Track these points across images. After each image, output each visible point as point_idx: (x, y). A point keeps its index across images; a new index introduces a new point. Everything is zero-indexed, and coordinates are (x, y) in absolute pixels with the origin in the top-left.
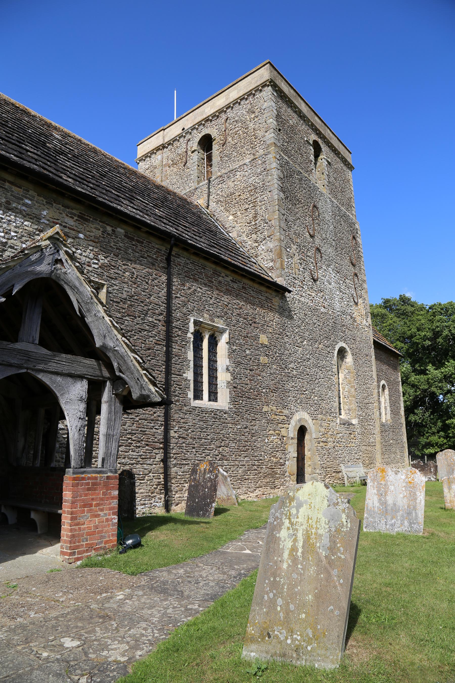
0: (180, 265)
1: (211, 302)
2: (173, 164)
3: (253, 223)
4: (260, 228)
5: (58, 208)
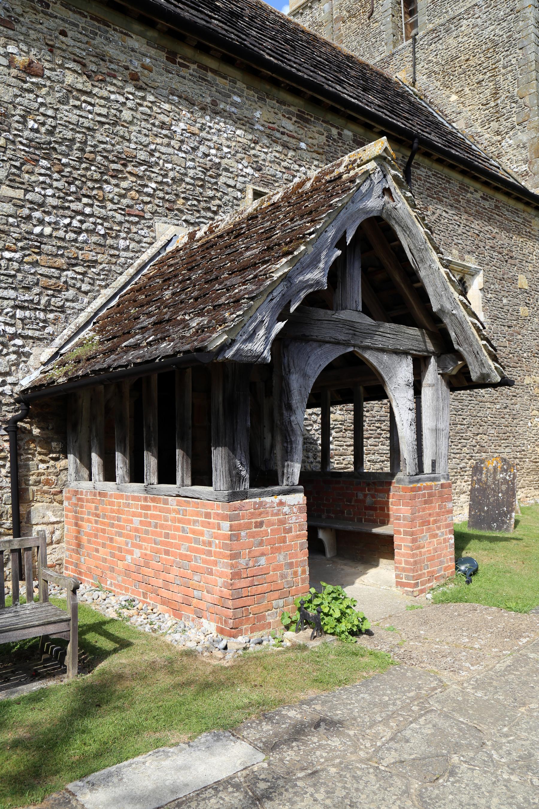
0: (421, 180)
1: (459, 232)
2: (350, 16)
3: (492, 104)
4: (505, 111)
5: (272, 105)
